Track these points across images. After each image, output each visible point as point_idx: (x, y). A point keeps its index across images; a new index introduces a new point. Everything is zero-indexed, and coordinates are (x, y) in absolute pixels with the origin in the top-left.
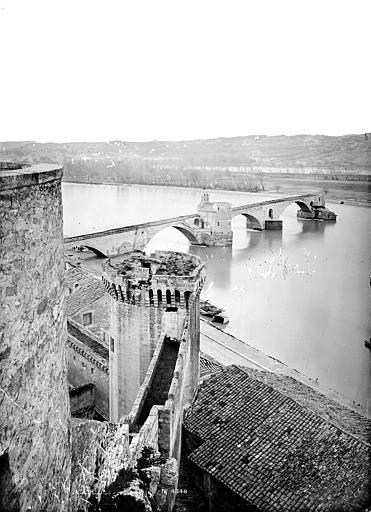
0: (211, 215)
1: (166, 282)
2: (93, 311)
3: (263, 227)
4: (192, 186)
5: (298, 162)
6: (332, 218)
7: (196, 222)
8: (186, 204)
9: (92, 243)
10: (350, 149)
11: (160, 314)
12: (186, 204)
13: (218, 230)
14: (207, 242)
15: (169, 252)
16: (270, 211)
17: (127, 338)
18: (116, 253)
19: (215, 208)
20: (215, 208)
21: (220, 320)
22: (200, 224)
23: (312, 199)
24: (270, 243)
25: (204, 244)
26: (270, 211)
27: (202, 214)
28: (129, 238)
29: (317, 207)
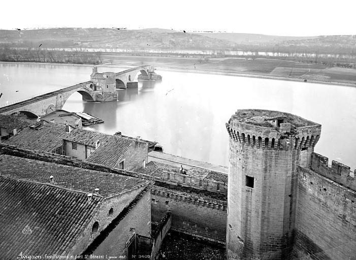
0: (102, 81)
1: (307, 131)
2: (124, 160)
3: (126, 87)
4: (48, 62)
5: (107, 45)
6: (160, 78)
7: (91, 86)
8: (84, 75)
9: (27, 108)
10: (137, 38)
11: (298, 154)
12: (84, 75)
13: (107, 91)
14: (99, 99)
15: (250, 110)
16: (130, 76)
17: (273, 175)
18: (45, 113)
19: (105, 76)
20: (105, 76)
21: (159, 149)
22: (93, 88)
23: (148, 68)
24: (130, 98)
25: (97, 101)
26: (130, 76)
27: (95, 81)
28: (52, 101)
29: (151, 72)
